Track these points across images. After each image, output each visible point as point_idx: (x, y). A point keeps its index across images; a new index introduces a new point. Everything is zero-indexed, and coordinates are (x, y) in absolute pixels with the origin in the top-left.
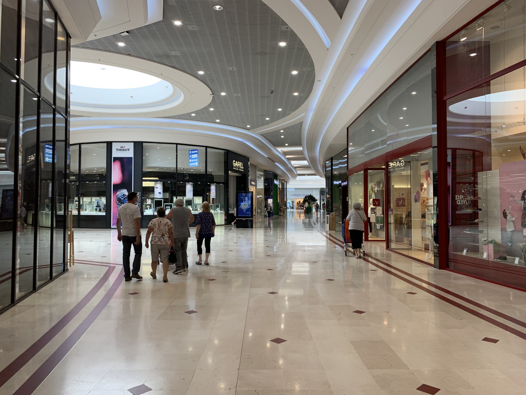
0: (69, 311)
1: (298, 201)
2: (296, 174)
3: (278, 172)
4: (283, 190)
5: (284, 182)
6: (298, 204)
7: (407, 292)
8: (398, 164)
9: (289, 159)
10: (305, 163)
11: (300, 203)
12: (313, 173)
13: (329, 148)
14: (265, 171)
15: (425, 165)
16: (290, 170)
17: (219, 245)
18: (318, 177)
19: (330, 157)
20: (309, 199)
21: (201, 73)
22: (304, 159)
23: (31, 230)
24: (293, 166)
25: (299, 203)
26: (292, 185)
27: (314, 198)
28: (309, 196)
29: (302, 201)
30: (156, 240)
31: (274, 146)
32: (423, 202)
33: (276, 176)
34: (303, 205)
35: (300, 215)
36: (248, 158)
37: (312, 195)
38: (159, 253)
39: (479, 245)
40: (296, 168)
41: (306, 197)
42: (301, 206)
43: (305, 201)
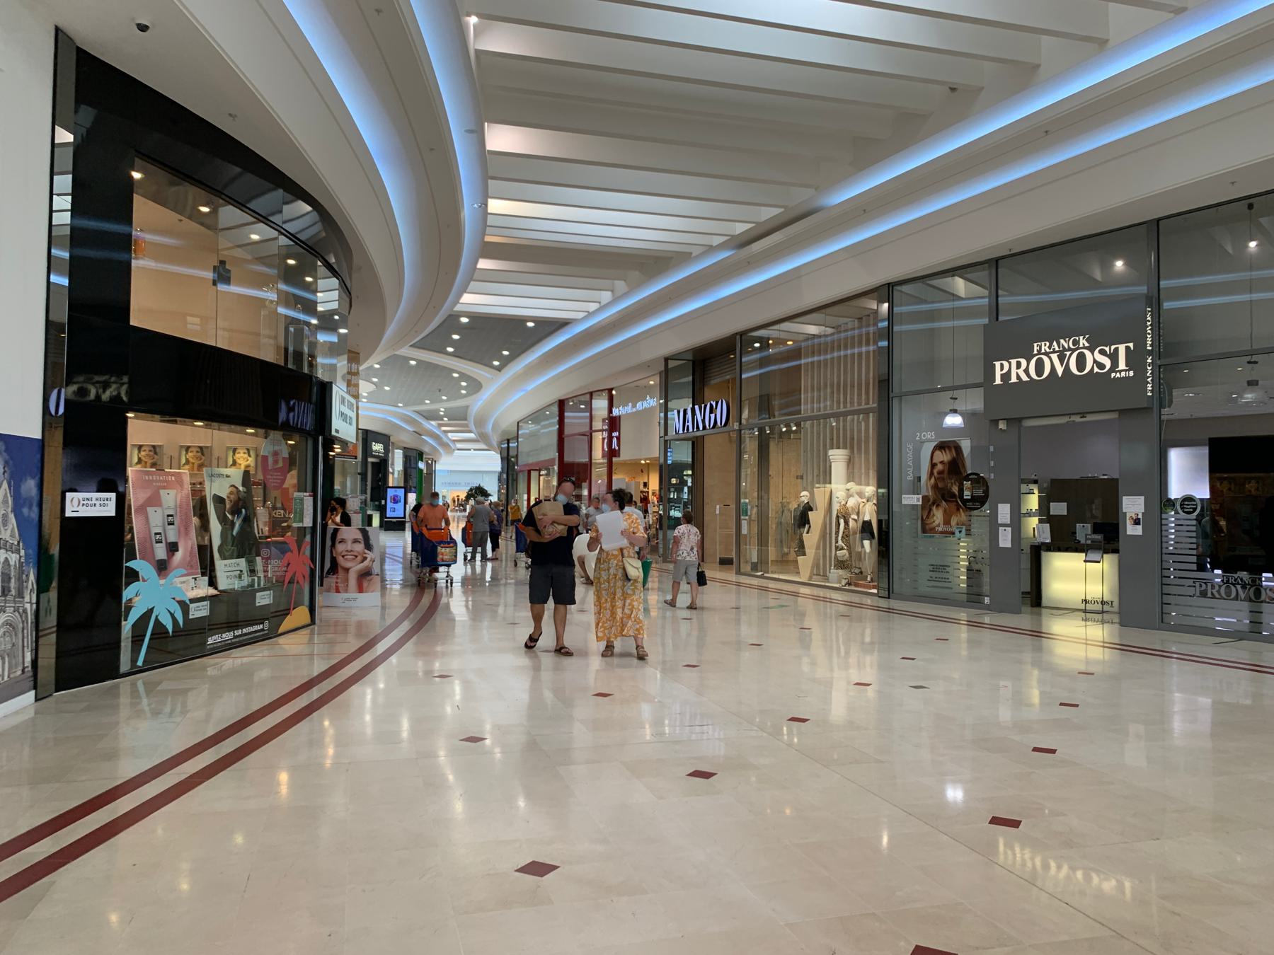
0: (372, 637)
1: (455, 496)
2: (453, 448)
3: (426, 449)
4: (431, 472)
5: (432, 463)
6: (454, 501)
7: (611, 697)
9: (446, 432)
10: (472, 435)
11: (458, 499)
12: (485, 447)
13: (502, 432)
14: (405, 448)
15: (258, 750)
16: (445, 445)
17: (742, 501)
18: (493, 452)
19: (506, 438)
20: (476, 493)
21: (375, 380)
22: (470, 432)
23: (660, 576)
24: (450, 440)
25: (456, 500)
26: (445, 465)
27: (487, 491)
28: (476, 487)
29: (463, 496)
30: (684, 555)
31: (427, 419)
32: (518, 562)
33: (420, 455)
34: (463, 503)
35: (458, 523)
36: (389, 437)
37: (481, 485)
38: (1122, 412)
39: (136, 559)
40: (454, 441)
41: (471, 490)
42: (460, 505)
43: (468, 497)
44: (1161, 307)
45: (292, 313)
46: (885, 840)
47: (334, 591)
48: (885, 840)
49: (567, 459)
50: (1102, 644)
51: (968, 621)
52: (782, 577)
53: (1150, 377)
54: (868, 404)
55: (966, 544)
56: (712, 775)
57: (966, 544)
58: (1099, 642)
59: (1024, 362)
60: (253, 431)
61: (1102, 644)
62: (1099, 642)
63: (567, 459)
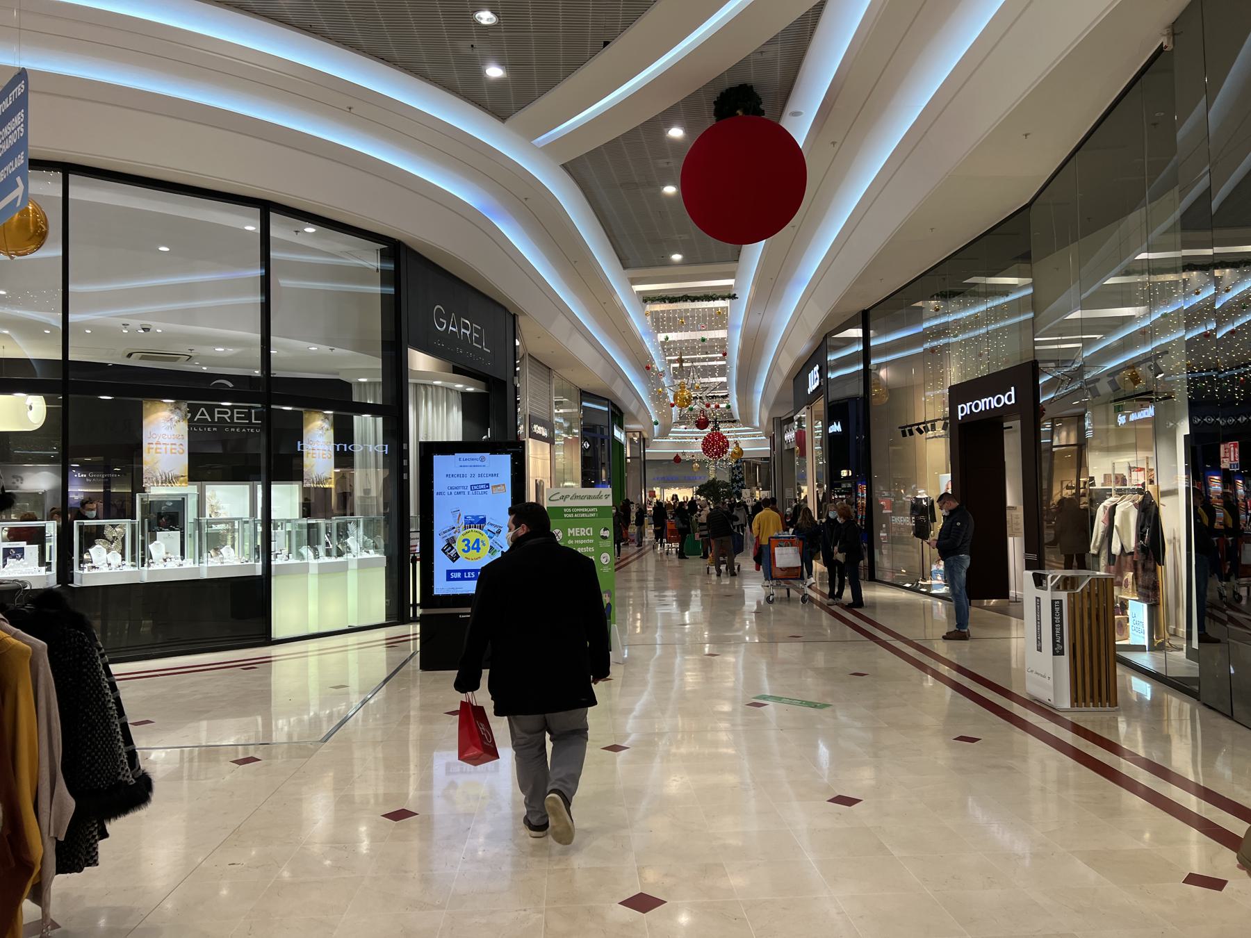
8: (203, 414)
44: (1136, 673)
45: (419, 681)
46: (583, 699)
47: (735, 264)
48: (583, 699)
49: (383, 620)
50: (273, 659)
51: (307, 656)
52: (88, 156)
53: (212, 416)
54: (218, 414)
55: (247, 410)
56: (857, 801)
57: (247, 410)
58: (275, 661)
59: (584, 529)
60: (223, 350)
61: (273, 659)
62: (275, 661)
63: (383, 620)
